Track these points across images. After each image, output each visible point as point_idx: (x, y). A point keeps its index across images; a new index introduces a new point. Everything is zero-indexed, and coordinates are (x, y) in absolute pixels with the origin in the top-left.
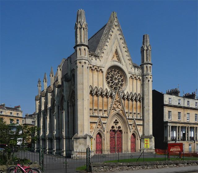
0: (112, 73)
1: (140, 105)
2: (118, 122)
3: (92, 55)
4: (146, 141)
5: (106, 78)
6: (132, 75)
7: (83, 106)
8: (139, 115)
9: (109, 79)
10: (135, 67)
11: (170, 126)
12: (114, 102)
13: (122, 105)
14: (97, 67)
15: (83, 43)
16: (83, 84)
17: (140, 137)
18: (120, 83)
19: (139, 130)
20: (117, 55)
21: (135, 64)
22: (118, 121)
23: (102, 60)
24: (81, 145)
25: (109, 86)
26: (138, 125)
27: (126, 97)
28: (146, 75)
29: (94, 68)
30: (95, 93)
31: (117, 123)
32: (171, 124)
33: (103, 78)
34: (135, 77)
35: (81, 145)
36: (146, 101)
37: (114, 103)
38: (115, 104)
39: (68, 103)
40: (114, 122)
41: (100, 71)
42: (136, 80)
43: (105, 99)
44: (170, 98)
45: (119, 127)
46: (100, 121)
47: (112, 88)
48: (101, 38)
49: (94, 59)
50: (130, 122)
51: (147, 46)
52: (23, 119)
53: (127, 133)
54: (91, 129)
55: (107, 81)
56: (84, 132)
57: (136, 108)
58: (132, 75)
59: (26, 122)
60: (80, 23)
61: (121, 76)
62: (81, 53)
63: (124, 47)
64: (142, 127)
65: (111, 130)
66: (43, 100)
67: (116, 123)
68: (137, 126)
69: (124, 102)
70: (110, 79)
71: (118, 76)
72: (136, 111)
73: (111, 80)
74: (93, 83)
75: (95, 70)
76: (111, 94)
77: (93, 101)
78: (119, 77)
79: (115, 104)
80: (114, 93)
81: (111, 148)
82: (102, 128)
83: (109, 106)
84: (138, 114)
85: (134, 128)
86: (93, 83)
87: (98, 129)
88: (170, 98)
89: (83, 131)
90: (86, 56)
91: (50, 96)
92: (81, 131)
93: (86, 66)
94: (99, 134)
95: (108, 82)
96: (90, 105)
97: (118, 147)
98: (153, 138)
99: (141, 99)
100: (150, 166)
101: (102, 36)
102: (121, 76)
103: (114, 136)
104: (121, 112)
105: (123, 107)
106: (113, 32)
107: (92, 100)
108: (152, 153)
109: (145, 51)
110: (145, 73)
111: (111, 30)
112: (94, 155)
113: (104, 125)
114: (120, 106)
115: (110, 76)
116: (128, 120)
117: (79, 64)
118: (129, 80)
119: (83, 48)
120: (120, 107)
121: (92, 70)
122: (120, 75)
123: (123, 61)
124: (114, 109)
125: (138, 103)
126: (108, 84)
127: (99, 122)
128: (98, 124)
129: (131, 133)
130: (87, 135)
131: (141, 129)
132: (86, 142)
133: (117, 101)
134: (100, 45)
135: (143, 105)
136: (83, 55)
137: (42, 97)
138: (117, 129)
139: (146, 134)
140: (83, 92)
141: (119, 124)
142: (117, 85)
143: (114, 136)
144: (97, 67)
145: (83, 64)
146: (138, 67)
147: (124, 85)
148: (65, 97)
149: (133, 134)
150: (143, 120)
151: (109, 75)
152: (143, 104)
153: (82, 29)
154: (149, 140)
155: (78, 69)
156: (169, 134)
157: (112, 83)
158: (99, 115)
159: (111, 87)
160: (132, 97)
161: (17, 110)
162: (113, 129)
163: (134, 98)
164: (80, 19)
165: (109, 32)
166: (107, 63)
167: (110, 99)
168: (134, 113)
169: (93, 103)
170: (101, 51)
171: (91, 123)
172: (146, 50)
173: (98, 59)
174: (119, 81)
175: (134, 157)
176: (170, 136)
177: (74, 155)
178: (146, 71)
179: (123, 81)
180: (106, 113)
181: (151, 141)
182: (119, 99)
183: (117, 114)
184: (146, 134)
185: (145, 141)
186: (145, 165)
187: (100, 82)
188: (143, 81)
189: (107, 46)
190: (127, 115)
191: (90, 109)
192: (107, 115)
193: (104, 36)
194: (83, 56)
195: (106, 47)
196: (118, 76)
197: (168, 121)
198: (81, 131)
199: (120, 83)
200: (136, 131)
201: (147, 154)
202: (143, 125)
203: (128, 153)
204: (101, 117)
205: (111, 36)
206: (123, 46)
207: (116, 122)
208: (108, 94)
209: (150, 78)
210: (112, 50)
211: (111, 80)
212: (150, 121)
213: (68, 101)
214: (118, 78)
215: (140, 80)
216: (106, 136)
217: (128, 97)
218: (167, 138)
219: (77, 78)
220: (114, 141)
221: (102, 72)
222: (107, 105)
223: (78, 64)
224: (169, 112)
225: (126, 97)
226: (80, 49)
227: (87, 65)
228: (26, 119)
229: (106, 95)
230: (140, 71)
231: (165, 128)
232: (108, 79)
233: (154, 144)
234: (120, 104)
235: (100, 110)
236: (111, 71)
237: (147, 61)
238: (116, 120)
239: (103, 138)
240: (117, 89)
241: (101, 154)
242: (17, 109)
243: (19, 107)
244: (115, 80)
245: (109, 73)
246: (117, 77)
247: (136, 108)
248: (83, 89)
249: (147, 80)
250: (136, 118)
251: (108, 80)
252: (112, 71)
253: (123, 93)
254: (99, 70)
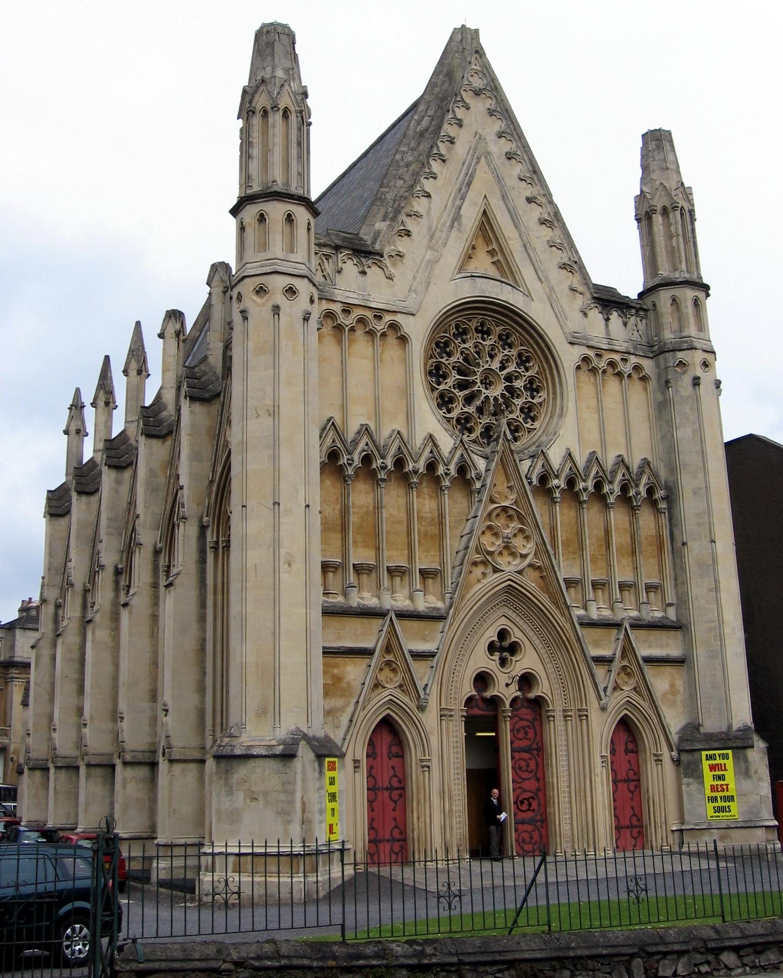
0: (464, 342)
2: (514, 648)
4: (712, 768)
5: (430, 373)
6: (591, 353)
7: (276, 543)
9: (450, 381)
13: (535, 537)
14: (369, 314)
16: (274, 412)
17: (674, 738)
18: (519, 402)
19: (664, 695)
20: (488, 241)
22: (516, 635)
23: (403, 272)
24: (261, 801)
25: (449, 420)
26: (648, 660)
28: (674, 350)
29: (348, 321)
33: (408, 374)
35: (261, 801)
36: (689, 506)
38: (490, 528)
39: (203, 529)
40: (492, 648)
45: (527, 680)
47: (470, 431)
49: (350, 268)
50: (597, 644)
53: (583, 715)
54: (328, 692)
55: (433, 389)
56: (277, 715)
58: (591, 353)
61: (523, 361)
63: (530, 200)
65: (469, 701)
67: (502, 649)
68: (648, 670)
69: (552, 516)
70: (454, 377)
73: (462, 386)
74: (344, 408)
75: (360, 332)
76: (462, 470)
77: (345, 512)
78: (511, 368)
80: (481, 464)
82: (409, 685)
86: (344, 408)
87: (383, 696)
90: (300, 255)
92: (262, 712)
93: (293, 309)
94: (387, 725)
95: (442, 396)
96: (325, 541)
98: (760, 745)
102: (523, 361)
104: (530, 582)
105: (541, 550)
106: (460, 126)
107: (338, 507)
111: (450, 116)
113: (420, 670)
114: (527, 538)
115: (453, 359)
118: (578, 380)
120: (528, 548)
121: (339, 328)
122: (514, 352)
123: (527, 273)
124: (485, 563)
126: (439, 406)
127: (388, 649)
128: (616, 665)
132: (288, 788)
133: (505, 509)
135: (677, 533)
141: (526, 661)
145: (280, 299)
147: (543, 410)
149: (625, 725)
151: (449, 355)
153: (678, 213)
154: (729, 763)
157: (469, 400)
159: (464, 424)
160: (598, 486)
163: (613, 489)
164: (269, 69)
165: (440, 127)
166: (432, 287)
169: (344, 529)
170: (390, 227)
171: (328, 652)
174: (511, 390)
175: (466, 899)
178: (675, 326)
181: (744, 771)
182: (513, 496)
184: (711, 724)
190: (571, 596)
191: (326, 567)
192: (440, 604)
193: (413, 144)
194: (280, 254)
195: (419, 205)
198: (262, 712)
199: (519, 402)
201: (713, 865)
204: (402, 615)
206: (528, 194)
207: (506, 644)
208: (441, 470)
211: (462, 386)
212: (727, 630)
215: (644, 379)
216: (434, 741)
217: (571, 482)
221: (403, 340)
225: (563, 486)
229: (599, 494)
232: (445, 377)
233: (765, 789)
236: (462, 333)
238: (503, 634)
239: (414, 754)
240: (497, 439)
244: (487, 383)
245: (447, 344)
249: (687, 380)
250: (634, 614)
251: (441, 387)
252: (465, 332)
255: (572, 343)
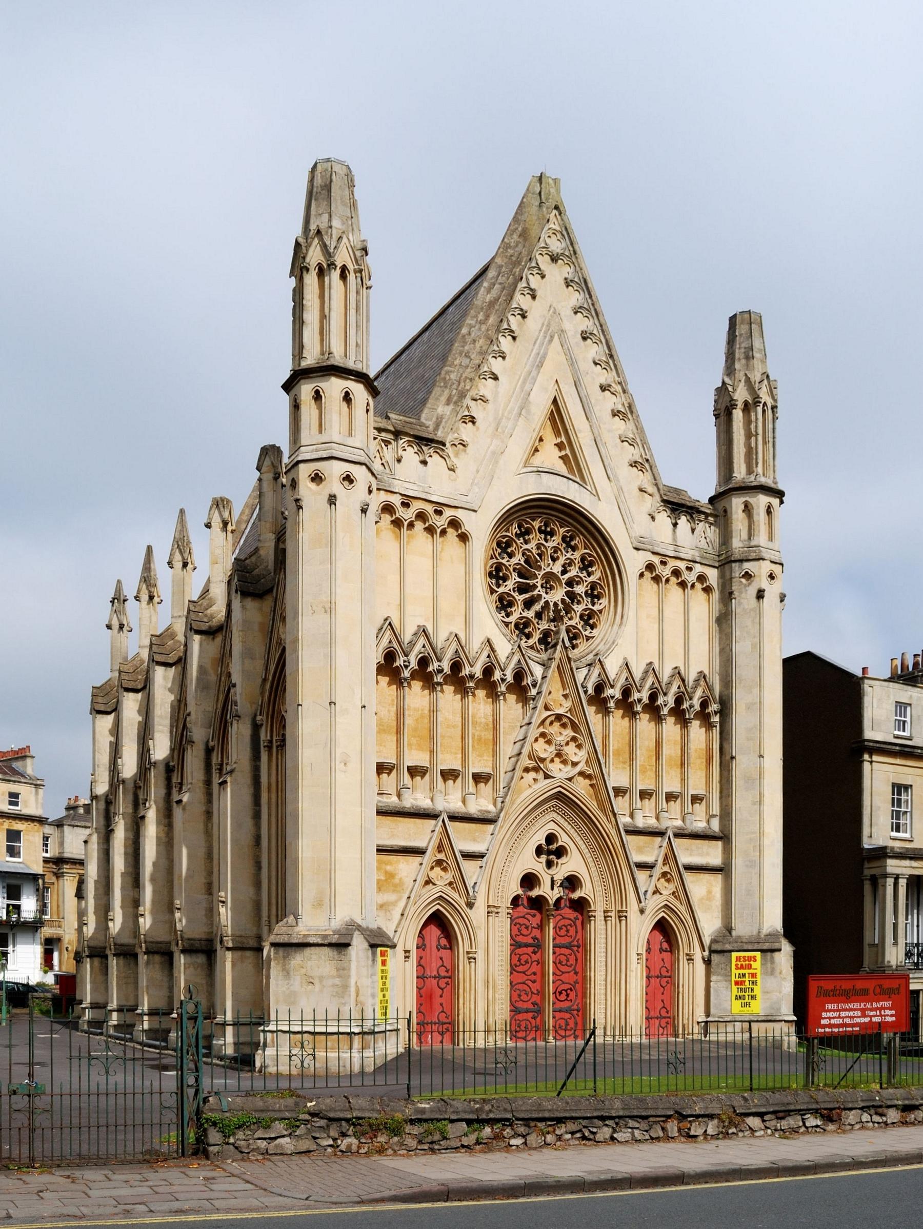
0: (526, 542)
1: (709, 742)
2: (561, 852)
3: (397, 434)
5: (490, 575)
6: (656, 560)
7: (331, 743)
8: (700, 808)
9: (510, 585)
10: (673, 510)
11: (897, 878)
12: (536, 721)
13: (587, 746)
14: (430, 509)
15: (338, 359)
16: (330, 609)
17: (707, 941)
20: (557, 433)
21: (677, 491)
22: (563, 839)
25: (507, 624)
26: (689, 868)
27: (615, 692)
28: (741, 561)
30: (414, 664)
31: (559, 857)
32: (907, 863)
33: (468, 573)
34: (676, 573)
35: (317, 986)
36: (741, 719)
37: (534, 732)
38: (543, 735)
39: (256, 728)
40: (539, 851)
41: (451, 532)
42: (680, 590)
43: (480, 704)
44: (902, 707)
45: (572, 882)
46: (670, 856)
47: (528, 636)
48: (460, 328)
49: (410, 455)
50: (640, 850)
51: (748, 380)
52: (48, 830)
53: (622, 916)
55: (492, 591)
56: (332, 905)
57: (683, 764)
58: (656, 560)
59: (62, 844)
60: (322, 240)
61: (586, 565)
62: (327, 418)
63: (603, 388)
64: (716, 881)
65: (516, 901)
66: (131, 704)
67: (549, 853)
68: (688, 877)
69: (606, 727)
70: (514, 579)
71: (570, 563)
72: (684, 781)
73: (522, 589)
74: (401, 607)
75: (419, 526)
76: (519, 675)
77: (400, 715)
78: (573, 572)
79: (543, 735)
80: (538, 670)
81: (515, 1010)
83: (507, 749)
84: (696, 799)
85: (667, 889)
86: (401, 607)
87: (432, 892)
88: (902, 707)
89: (326, 901)
91: (163, 678)
92: (318, 904)
94: (437, 920)
95: (501, 598)
97: (566, 1005)
99: (714, 707)
100: (631, 1123)
101: (469, 321)
102: (586, 565)
103: (536, 933)
104: (581, 788)
105: (595, 758)
106: (534, 297)
107: (394, 708)
108: (777, 1045)
109: (738, 414)
110: (737, 544)
111: (523, 284)
112: (401, 1050)
113: (469, 867)
114: (579, 747)
115: (514, 560)
116: (630, 840)
117: (313, 486)
119: (334, 387)
121: (397, 523)
122: (577, 555)
123: (595, 469)
124: (536, 769)
125: (696, 729)
127: (440, 849)
128: (428, 858)
129: (648, 922)
130: (352, 927)
131: (709, 892)
132: (343, 972)
133: (559, 717)
134: (453, 376)
135: (726, 746)
136: (335, 430)
137: (128, 690)
138: (557, 893)
139: (742, 929)
140: (331, 658)
142: (557, 619)
143: (536, 933)
144: (430, 509)
146: (690, 510)
148: (238, 689)
149: (662, 927)
150: (724, 837)
151: (511, 556)
152: (725, 736)
153: (336, 274)
154: (757, 965)
155: (306, 515)
156: (895, 926)
158: (665, 824)
159: (522, 628)
160: (653, 697)
161: (15, 772)
162: (534, 893)
163: (667, 701)
164: (326, 216)
165: (511, 297)
167: (510, 707)
168: (670, 797)
169: (399, 731)
172: (747, 408)
173: (435, 461)
174: (572, 596)
176: (901, 941)
177: (266, 1057)
178: (745, 535)
179: (599, 597)
180: (486, 789)
182: (568, 704)
183: (559, 796)
184: (742, 929)
185: (733, 967)
186: (602, 1118)
187: (450, 604)
188: (727, 596)
189: (496, 378)
190: (621, 805)
191: (382, 768)
192: (491, 808)
193: (481, 317)
195: (486, 387)
196: (570, 563)
197: (891, 844)
198: (318, 904)
199: (578, 608)
200: (682, 909)
201: (739, 1053)
202: (724, 870)
203: (628, 1040)
204: (453, 818)
205: (524, 316)
207: (554, 847)
208: (497, 675)
209: (772, 577)
210: (525, 405)
211: (522, 589)
212: (766, 842)
213: (259, 718)
214: (566, 576)
215: (707, 590)
216: (481, 936)
217: (626, 692)
218: (880, 948)
219: (297, 572)
220: (535, 968)
221: (464, 538)
222: (495, 741)
223: (306, 488)
224: (899, 789)
226: (317, 396)
227: (359, 493)
228: (66, 827)
230: (712, 533)
231: (867, 887)
232: (505, 579)
234: (574, 739)
235: (449, 775)
236: (524, 533)
237: (750, 471)
238: (551, 838)
239: (463, 946)
240: (555, 646)
241: (448, 1046)
242: (17, 765)
243: (22, 755)
244: (548, 588)
245: (508, 544)
246: (557, 568)
247: (683, 764)
248: (331, 640)
249: (752, 591)
250: (679, 823)
251: (501, 590)
252: (528, 532)
253: (596, 671)
254: (440, 522)
255: (637, 549)
